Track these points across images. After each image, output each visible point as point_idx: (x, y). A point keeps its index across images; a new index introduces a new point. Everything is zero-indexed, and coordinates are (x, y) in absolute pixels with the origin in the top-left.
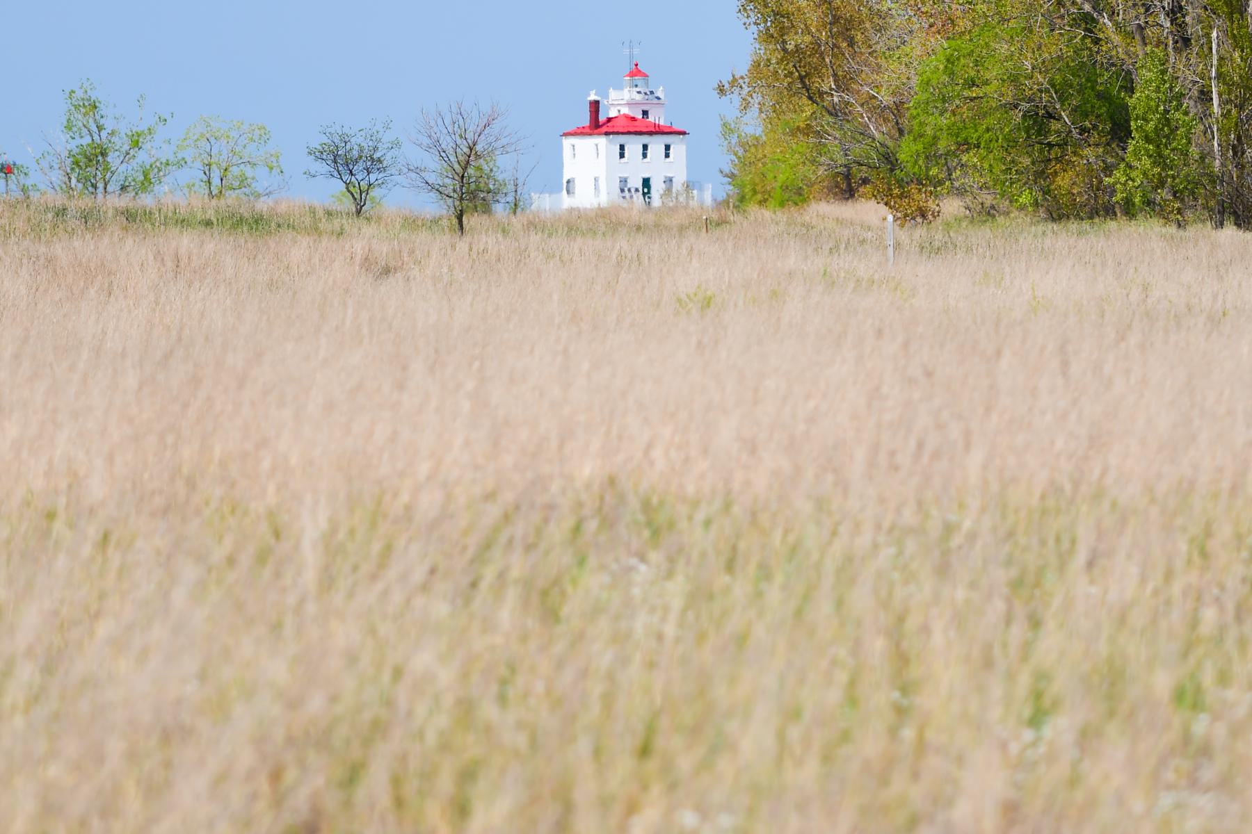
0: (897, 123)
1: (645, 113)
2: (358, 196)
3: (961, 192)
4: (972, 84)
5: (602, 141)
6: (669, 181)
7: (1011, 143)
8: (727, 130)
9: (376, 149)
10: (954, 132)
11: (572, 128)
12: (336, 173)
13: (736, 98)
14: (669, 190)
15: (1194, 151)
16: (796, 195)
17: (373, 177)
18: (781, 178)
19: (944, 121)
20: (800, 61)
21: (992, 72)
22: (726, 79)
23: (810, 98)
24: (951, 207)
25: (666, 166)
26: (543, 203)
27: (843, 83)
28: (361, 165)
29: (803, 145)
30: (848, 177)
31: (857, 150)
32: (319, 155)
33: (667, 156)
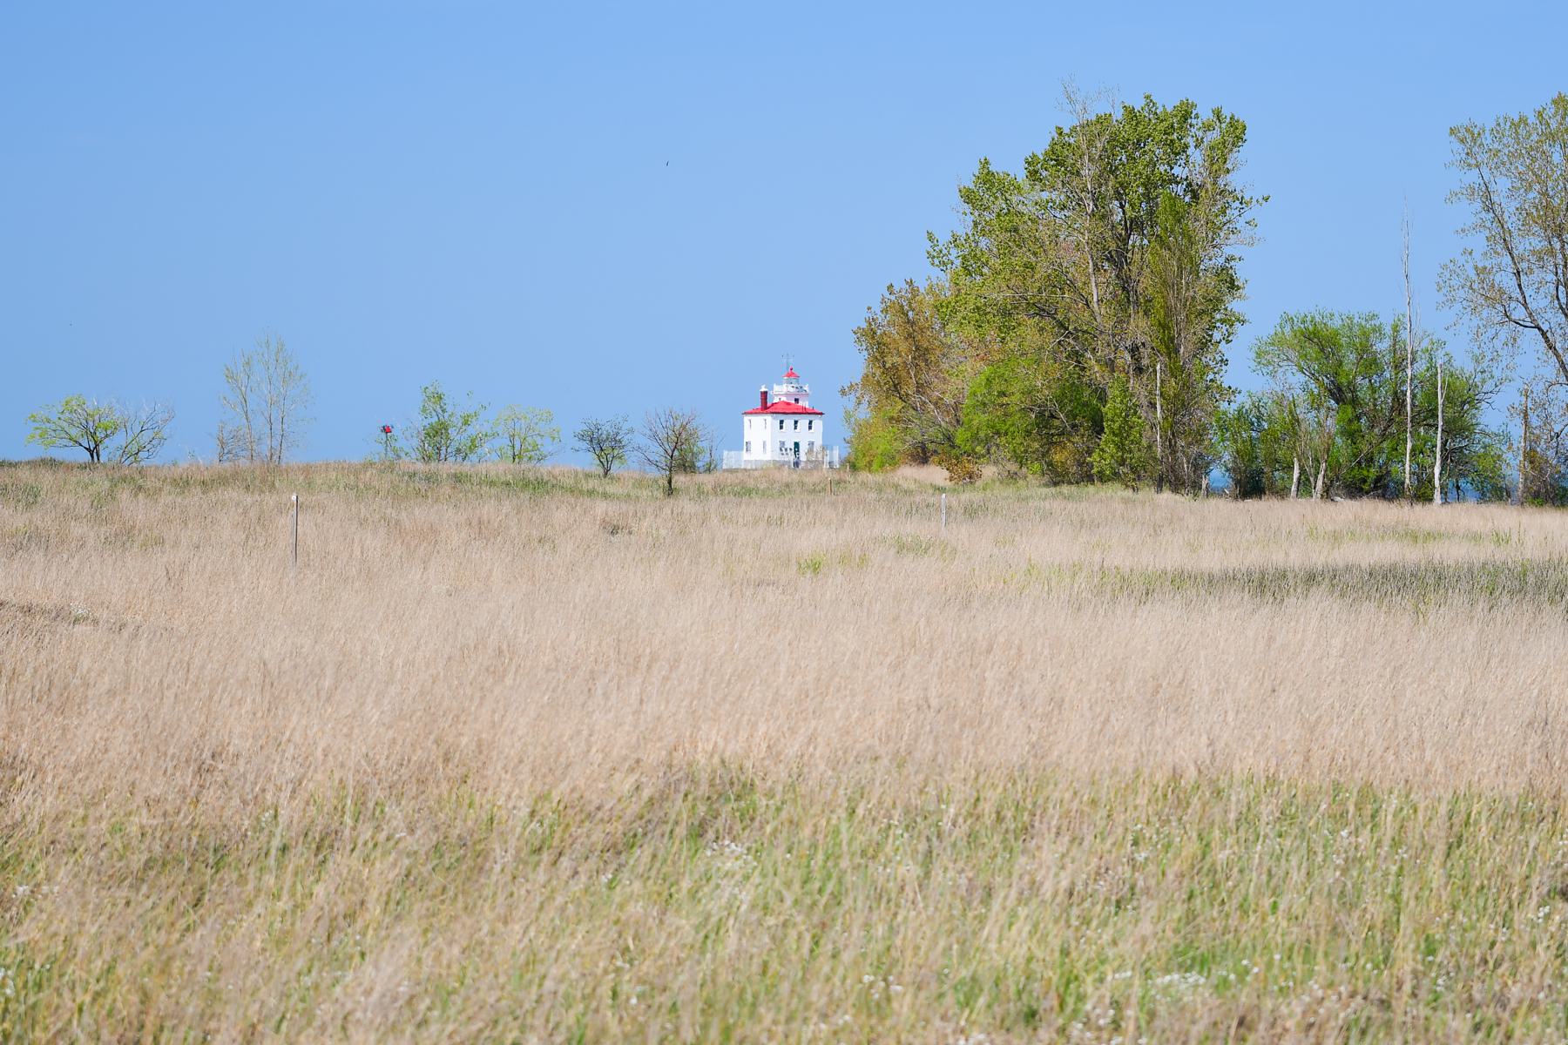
3: (996, 463)
5: (769, 418)
6: (811, 444)
8: (848, 417)
13: (852, 398)
15: (1144, 443)
16: (891, 461)
19: (985, 417)
22: (846, 385)
24: (989, 471)
25: (809, 435)
27: (920, 388)
29: (896, 429)
30: (924, 449)
32: (582, 438)
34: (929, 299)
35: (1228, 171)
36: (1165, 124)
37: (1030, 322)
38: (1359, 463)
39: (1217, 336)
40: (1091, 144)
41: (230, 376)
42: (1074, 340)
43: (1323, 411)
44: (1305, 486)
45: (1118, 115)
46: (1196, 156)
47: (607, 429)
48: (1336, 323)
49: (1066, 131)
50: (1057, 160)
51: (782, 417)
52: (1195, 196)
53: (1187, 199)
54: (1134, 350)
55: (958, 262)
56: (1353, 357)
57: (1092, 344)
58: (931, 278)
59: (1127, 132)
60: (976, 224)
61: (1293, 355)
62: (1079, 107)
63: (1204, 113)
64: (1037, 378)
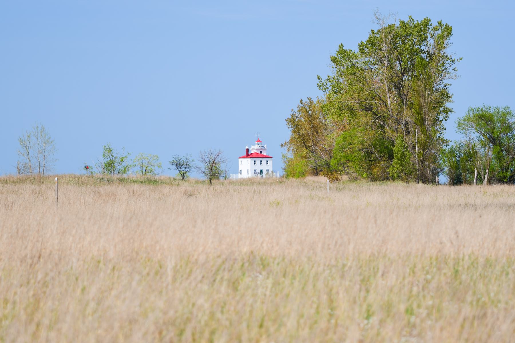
1: (261, 152)
3: (347, 174)
5: (249, 159)
6: (268, 170)
7: (361, 160)
8: (284, 156)
9: (188, 162)
13: (286, 148)
14: (268, 173)
15: (411, 162)
16: (302, 175)
17: (187, 169)
18: (298, 170)
19: (343, 154)
21: (356, 141)
22: (283, 143)
24: (345, 178)
25: (267, 166)
26: (233, 177)
27: (315, 144)
29: (304, 161)
30: (316, 169)
31: (319, 162)
32: (172, 163)
33: (255, 164)
34: (318, 106)
35: (445, 47)
36: (418, 28)
37: (362, 113)
38: (503, 170)
39: (441, 118)
40: (386, 37)
41: (22, 142)
42: (380, 119)
43: (487, 148)
44: (480, 180)
45: (398, 24)
46: (431, 41)
47: (183, 160)
48: (492, 111)
49: (376, 31)
50: (372, 44)
51: (255, 159)
52: (431, 59)
53: (427, 60)
54: (406, 124)
55: (330, 88)
56: (499, 125)
57: (386, 121)
58: (319, 96)
59: (402, 32)
60: (338, 72)
61: (474, 125)
62: (381, 22)
63: (434, 23)
64: (363, 134)
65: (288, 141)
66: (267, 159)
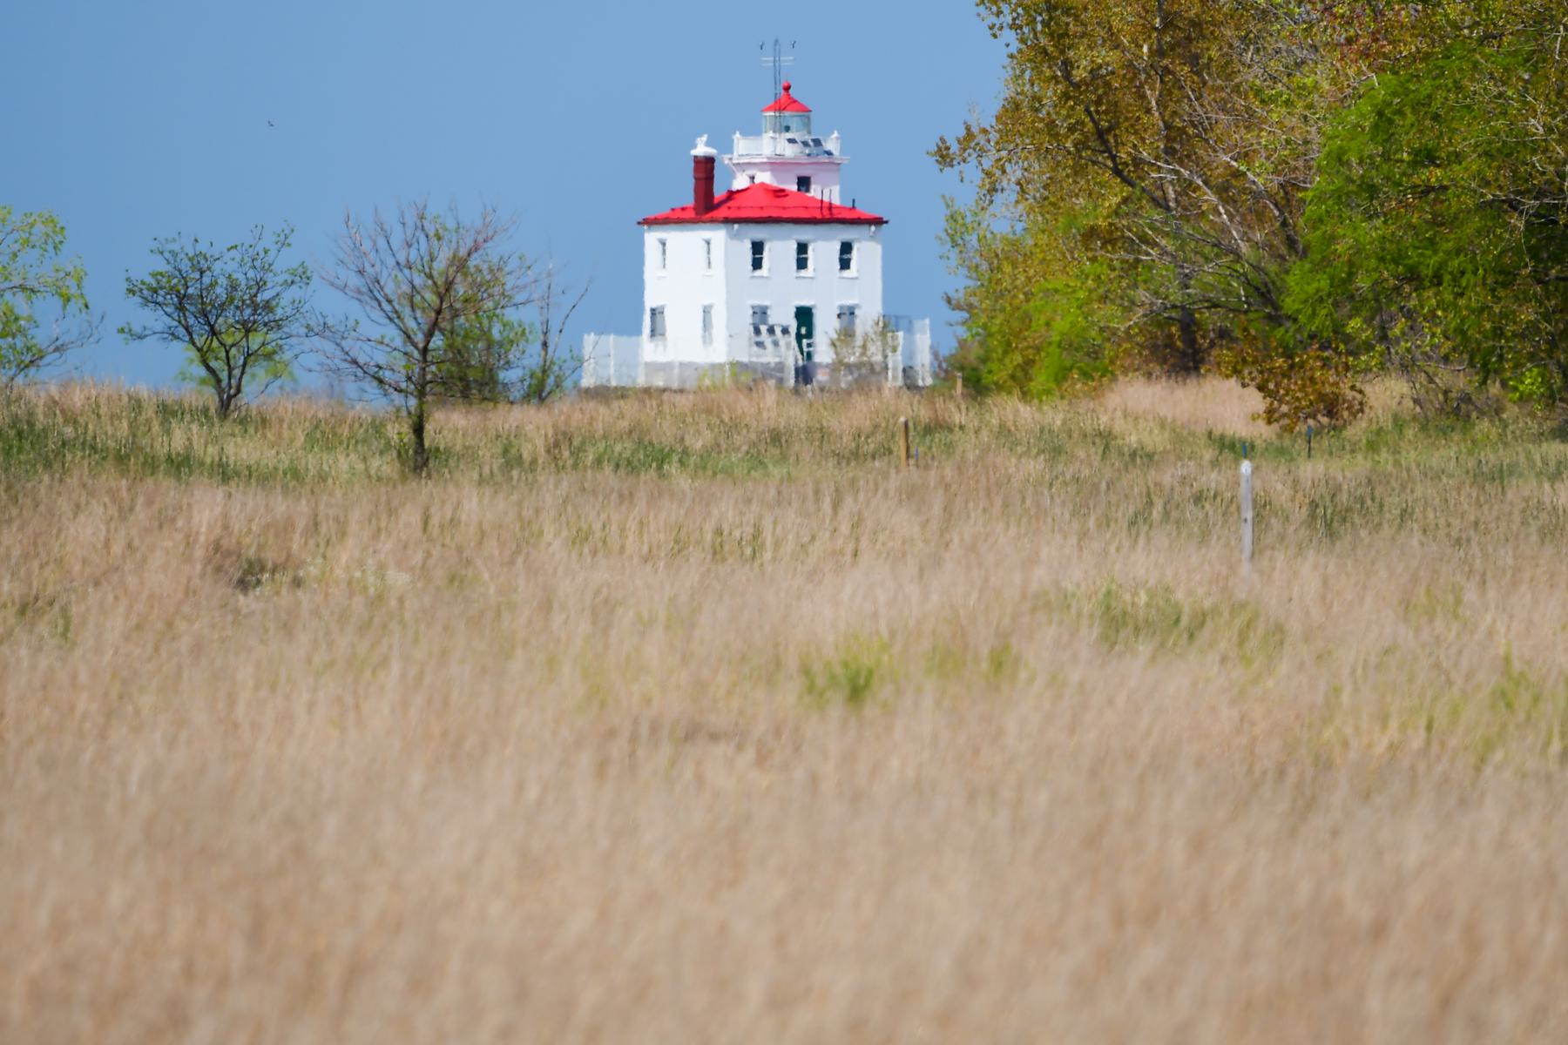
0: (1284, 224)
1: (804, 182)
2: (224, 376)
4: (1427, 157)
6: (847, 314)
7: (1505, 277)
8: (957, 229)
9: (260, 285)
10: (1390, 255)
11: (663, 210)
12: (182, 331)
13: (972, 171)
14: (847, 333)
16: (1089, 363)
17: (255, 341)
18: (1061, 325)
20: (1098, 102)
21: (1467, 136)
23: (1117, 172)
24: (1387, 393)
25: (844, 286)
26: (602, 359)
28: (231, 316)
29: (1103, 265)
30: (1189, 325)
31: (1209, 273)
32: (150, 294)
33: (757, 264)
47: (228, 268)
51: (758, 232)
65: (988, 121)
66: (848, 233)
